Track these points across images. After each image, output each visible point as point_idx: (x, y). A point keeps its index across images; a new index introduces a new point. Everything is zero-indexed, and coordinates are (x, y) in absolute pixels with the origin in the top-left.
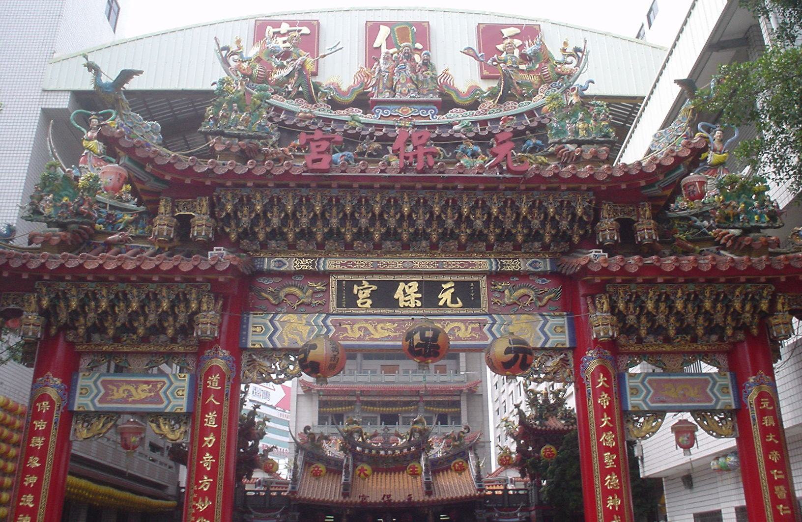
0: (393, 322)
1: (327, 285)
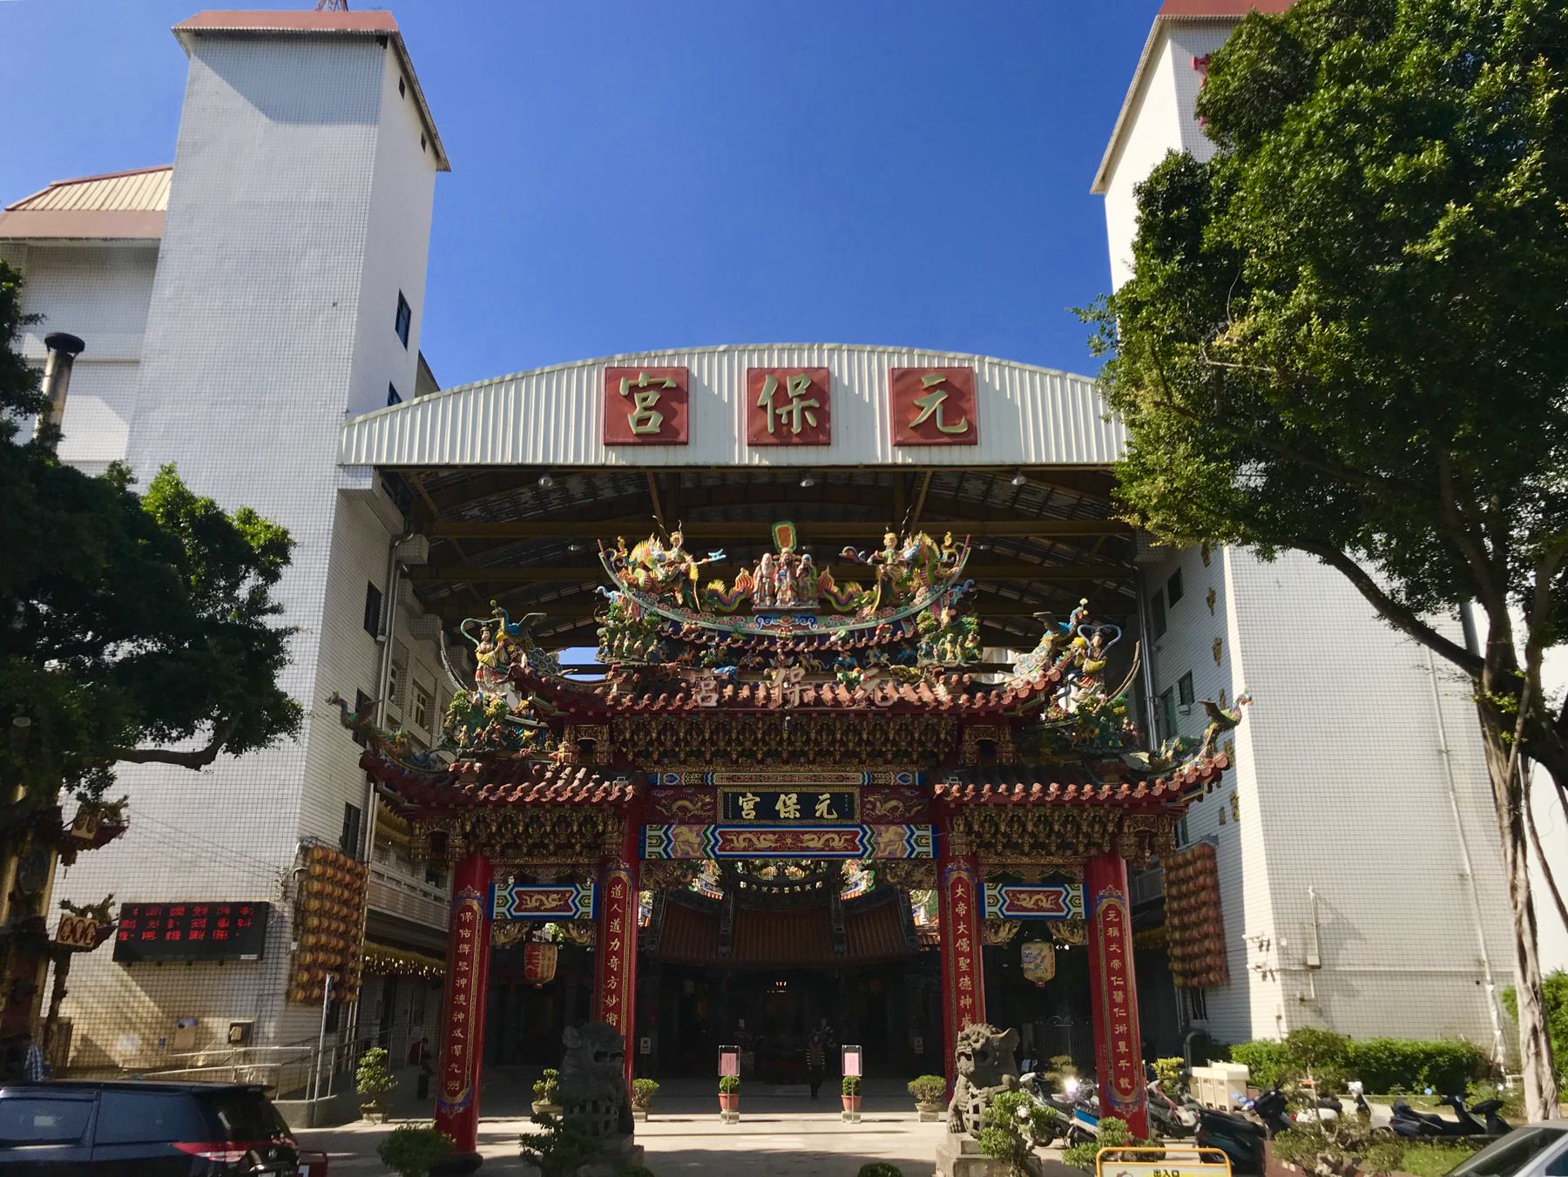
0: (774, 833)
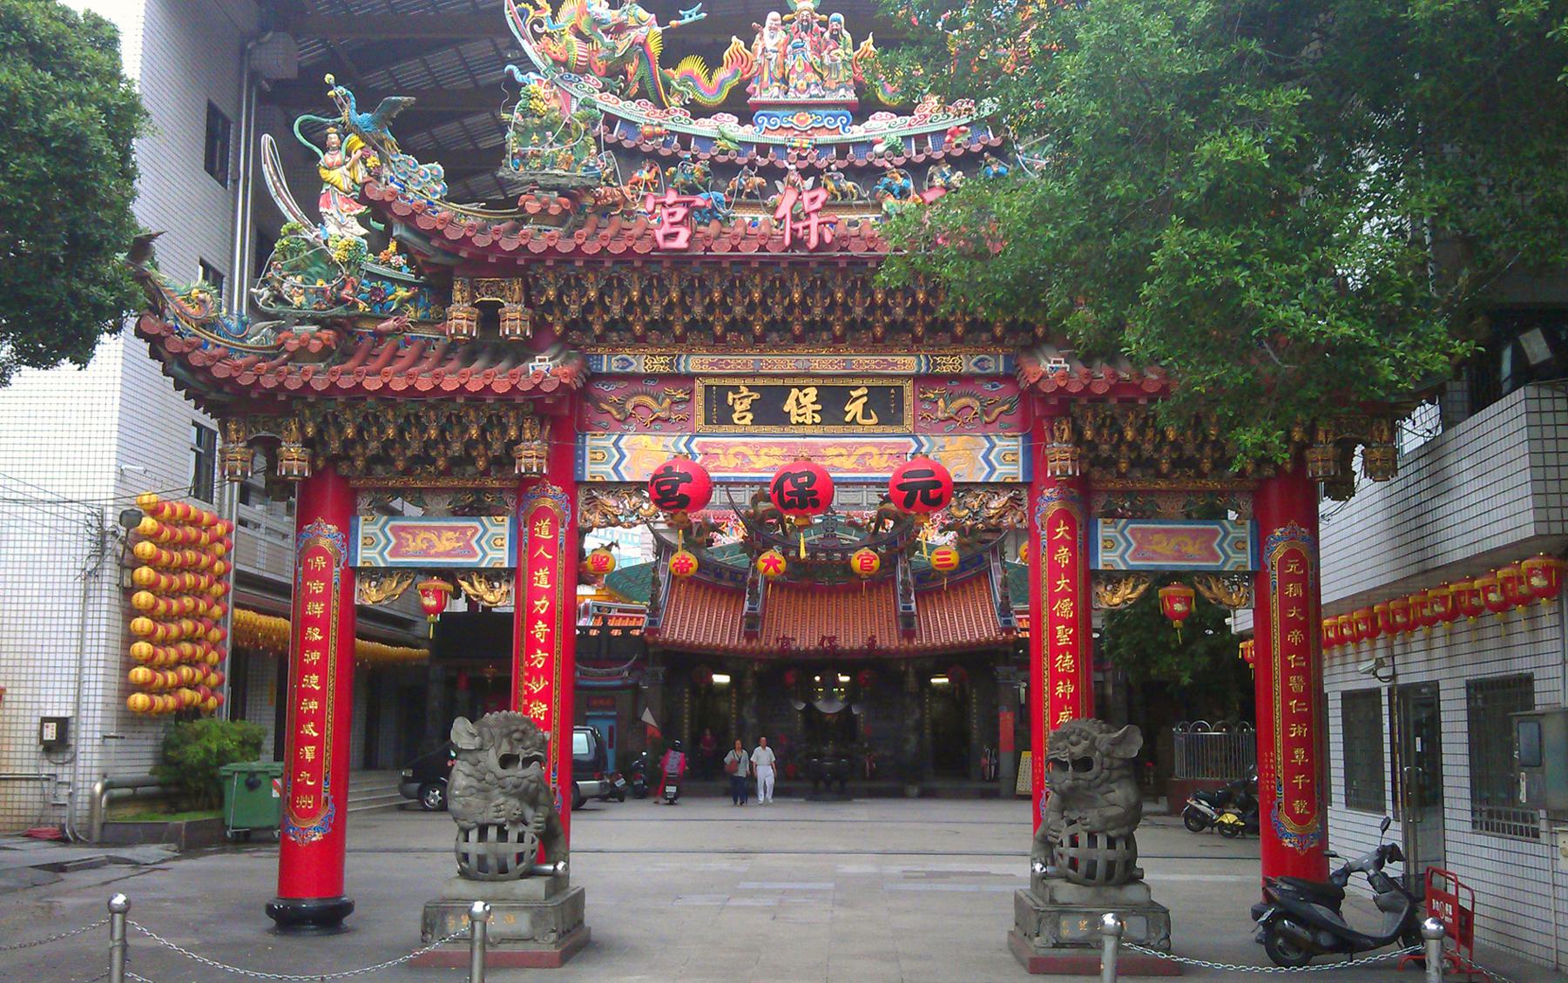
1: (692, 392)
